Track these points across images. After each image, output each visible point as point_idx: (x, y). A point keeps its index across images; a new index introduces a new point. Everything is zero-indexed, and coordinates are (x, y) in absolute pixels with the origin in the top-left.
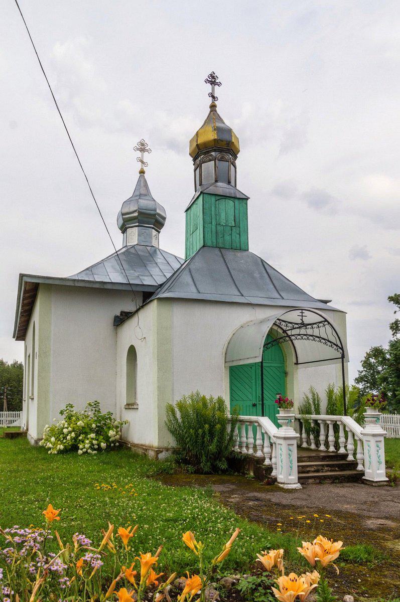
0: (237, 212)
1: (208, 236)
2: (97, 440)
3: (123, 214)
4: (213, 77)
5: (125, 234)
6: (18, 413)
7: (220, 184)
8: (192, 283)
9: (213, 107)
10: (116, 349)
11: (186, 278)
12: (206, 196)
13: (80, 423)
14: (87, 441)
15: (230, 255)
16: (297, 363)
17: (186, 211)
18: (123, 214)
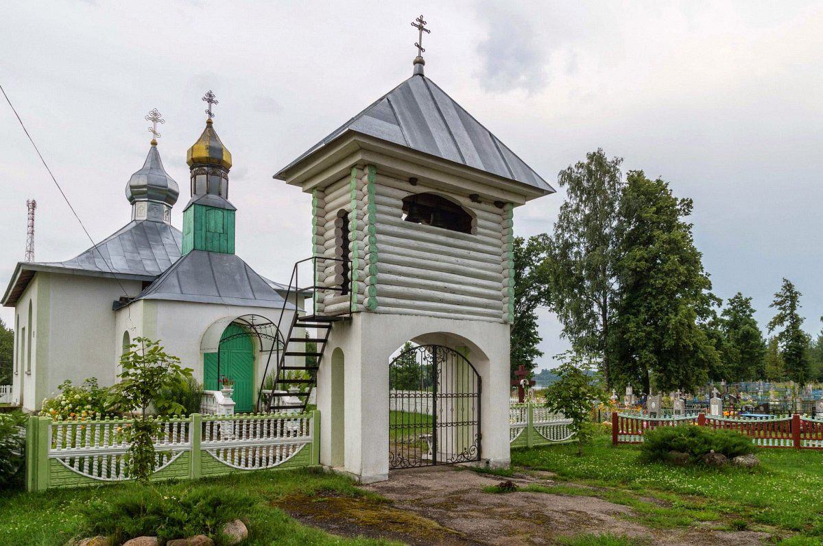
0: (226, 220)
1: (198, 241)
2: (93, 410)
3: (132, 187)
4: (210, 96)
5: (134, 206)
6: (5, 387)
7: (210, 196)
8: (178, 284)
9: (209, 123)
10: (115, 331)
11: (173, 280)
12: (199, 208)
13: (77, 396)
14: (83, 411)
15: (215, 257)
16: (261, 351)
17: (184, 212)
18: (132, 187)
